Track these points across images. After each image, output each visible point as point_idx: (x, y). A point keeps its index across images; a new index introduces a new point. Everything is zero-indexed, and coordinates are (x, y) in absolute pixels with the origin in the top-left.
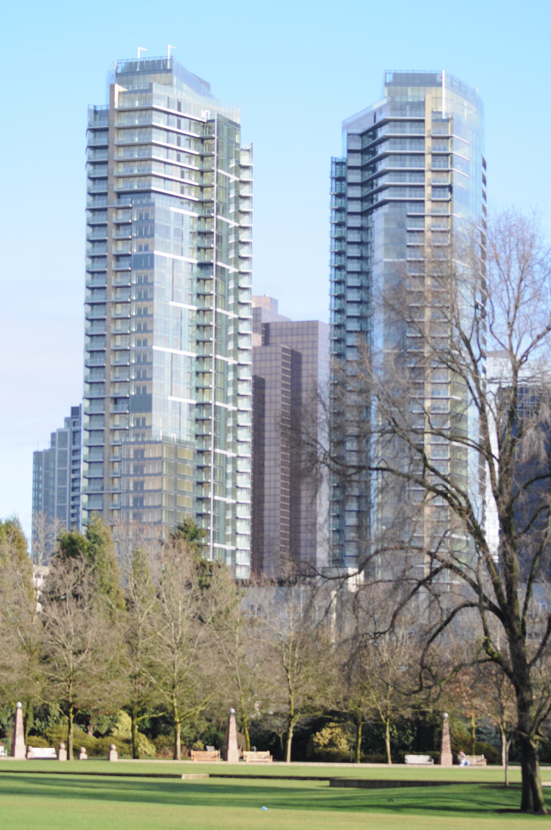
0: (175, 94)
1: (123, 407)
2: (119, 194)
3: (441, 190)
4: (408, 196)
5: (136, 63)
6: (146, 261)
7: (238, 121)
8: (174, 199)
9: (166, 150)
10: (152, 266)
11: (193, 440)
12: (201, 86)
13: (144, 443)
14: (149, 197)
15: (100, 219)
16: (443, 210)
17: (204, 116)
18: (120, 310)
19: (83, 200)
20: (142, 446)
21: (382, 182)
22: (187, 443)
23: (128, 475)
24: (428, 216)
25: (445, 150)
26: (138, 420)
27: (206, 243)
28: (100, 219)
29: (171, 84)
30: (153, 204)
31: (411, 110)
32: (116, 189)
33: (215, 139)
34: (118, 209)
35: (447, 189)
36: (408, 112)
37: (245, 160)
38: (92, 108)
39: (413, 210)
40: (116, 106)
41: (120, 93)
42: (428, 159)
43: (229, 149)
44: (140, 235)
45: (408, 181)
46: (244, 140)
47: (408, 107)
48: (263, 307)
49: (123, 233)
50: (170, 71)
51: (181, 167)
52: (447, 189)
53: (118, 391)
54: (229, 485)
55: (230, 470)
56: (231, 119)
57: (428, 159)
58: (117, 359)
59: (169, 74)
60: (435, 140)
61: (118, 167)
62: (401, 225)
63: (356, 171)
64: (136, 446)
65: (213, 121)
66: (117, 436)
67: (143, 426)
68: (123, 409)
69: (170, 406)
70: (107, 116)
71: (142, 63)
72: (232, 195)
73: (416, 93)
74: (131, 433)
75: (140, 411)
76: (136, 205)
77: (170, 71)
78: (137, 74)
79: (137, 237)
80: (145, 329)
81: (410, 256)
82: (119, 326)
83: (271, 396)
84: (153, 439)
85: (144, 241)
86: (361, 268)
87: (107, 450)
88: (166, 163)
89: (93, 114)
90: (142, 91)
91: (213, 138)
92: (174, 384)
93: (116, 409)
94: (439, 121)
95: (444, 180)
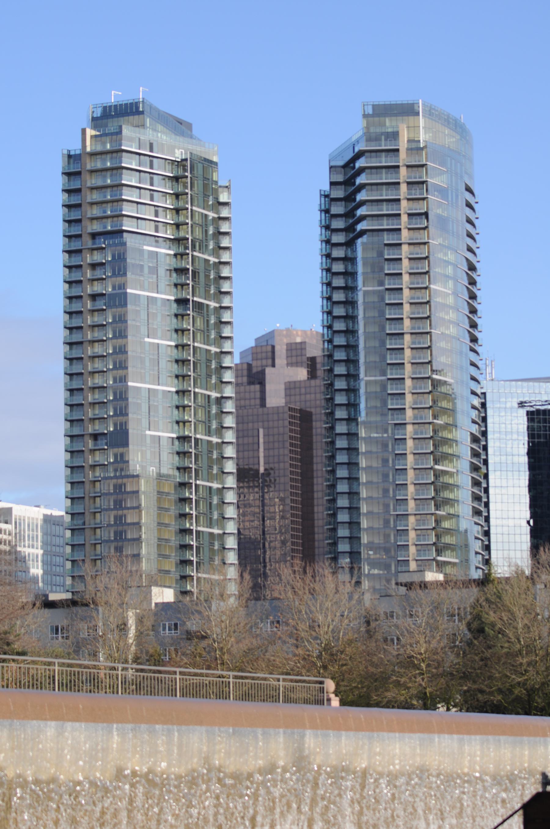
0: (148, 135)
1: (102, 443)
2: (94, 236)
3: (418, 217)
4: (385, 224)
5: (110, 107)
6: (120, 299)
7: (215, 159)
8: (148, 237)
9: (138, 190)
10: (125, 305)
11: (177, 473)
12: (180, 127)
13: (122, 477)
14: (122, 237)
15: (76, 260)
16: (422, 237)
17: (178, 155)
18: (98, 349)
19: (58, 242)
20: (120, 481)
21: (361, 212)
22: (168, 476)
23: (109, 509)
24: (405, 243)
25: (420, 178)
26: (116, 456)
27: (183, 280)
28: (76, 260)
29: (143, 126)
30: (125, 244)
31: (386, 140)
32: (89, 230)
33: (193, 179)
34: (93, 249)
35: (424, 217)
36: (383, 143)
37: (223, 198)
38: (65, 152)
39: (388, 239)
40: (88, 149)
41: (92, 137)
42: (404, 187)
43: (205, 186)
44: (114, 274)
45: (385, 210)
46: (220, 177)
47: (383, 138)
48: (307, 340)
49: (99, 273)
50: (142, 113)
51: (155, 206)
52: (424, 217)
53: (98, 427)
54: (215, 516)
55: (215, 501)
56: (207, 157)
57: (404, 187)
58: (97, 396)
59: (141, 116)
60: (410, 169)
61: (92, 208)
62: (380, 254)
63: (339, 203)
64: (115, 481)
65: (186, 160)
66: (98, 472)
67: (122, 461)
68: (102, 445)
69: (148, 441)
70: (80, 160)
71: (116, 106)
72: (211, 231)
73: (394, 124)
74: (111, 469)
75: (117, 445)
76: (109, 245)
77: (142, 113)
78: (112, 117)
79: (111, 277)
80: (122, 366)
81: (389, 284)
82: (98, 365)
83: (316, 428)
84: (131, 472)
85: (119, 280)
86: (346, 298)
87: (87, 486)
88: (138, 203)
89: (66, 159)
90: (112, 134)
91: (187, 177)
92: (151, 418)
93: (95, 445)
94: (415, 148)
95: (421, 207)
